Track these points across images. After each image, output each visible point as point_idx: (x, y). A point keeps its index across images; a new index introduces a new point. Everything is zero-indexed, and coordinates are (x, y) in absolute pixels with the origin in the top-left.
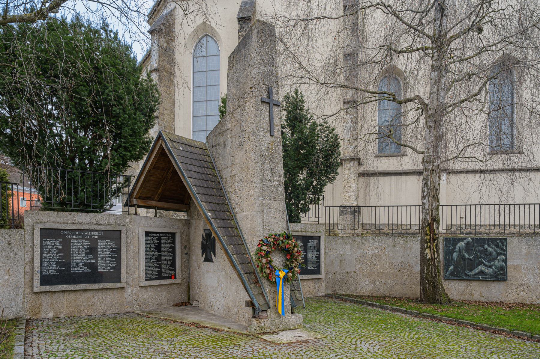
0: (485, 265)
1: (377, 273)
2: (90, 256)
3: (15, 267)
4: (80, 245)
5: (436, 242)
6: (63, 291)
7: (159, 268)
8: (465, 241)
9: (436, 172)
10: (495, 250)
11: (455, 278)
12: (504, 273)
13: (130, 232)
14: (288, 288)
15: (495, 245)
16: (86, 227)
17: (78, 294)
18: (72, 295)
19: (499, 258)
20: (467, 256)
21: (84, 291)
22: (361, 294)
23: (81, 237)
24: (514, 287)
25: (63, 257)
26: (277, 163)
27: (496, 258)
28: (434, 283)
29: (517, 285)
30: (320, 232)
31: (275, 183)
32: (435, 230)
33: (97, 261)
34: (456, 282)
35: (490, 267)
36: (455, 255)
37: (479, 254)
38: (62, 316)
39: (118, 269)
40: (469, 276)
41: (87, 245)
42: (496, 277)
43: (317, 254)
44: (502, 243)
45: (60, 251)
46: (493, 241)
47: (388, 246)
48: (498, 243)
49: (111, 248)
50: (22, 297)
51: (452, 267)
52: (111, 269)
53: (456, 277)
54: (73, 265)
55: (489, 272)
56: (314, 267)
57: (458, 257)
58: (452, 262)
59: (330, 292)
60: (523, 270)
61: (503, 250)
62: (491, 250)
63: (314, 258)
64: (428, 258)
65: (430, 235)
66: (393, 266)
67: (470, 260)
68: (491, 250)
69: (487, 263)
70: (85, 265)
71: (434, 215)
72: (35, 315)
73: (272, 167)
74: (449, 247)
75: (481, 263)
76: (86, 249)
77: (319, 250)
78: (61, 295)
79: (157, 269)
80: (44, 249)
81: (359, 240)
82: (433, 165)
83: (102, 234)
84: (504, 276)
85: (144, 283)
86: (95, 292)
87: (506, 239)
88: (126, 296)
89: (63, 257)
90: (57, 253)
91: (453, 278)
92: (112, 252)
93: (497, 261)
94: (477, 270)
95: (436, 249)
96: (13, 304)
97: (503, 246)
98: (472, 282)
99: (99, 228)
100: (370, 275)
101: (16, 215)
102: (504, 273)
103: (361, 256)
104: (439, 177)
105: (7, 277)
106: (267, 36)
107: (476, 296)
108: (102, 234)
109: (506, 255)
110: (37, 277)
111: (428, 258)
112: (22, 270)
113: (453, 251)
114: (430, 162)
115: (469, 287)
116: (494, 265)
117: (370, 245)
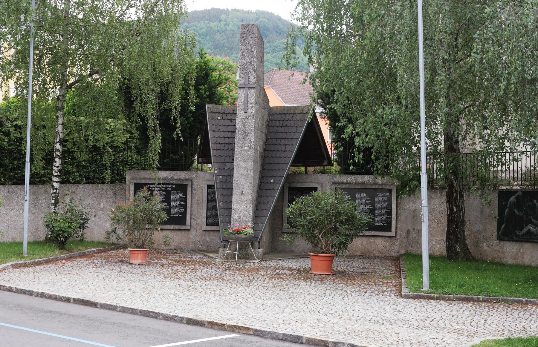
2: (166, 204)
8: (516, 195)
13: (196, 186)
39: (184, 214)
41: (164, 195)
43: (387, 209)
49: (180, 198)
52: (180, 214)
56: (383, 223)
63: (383, 213)
76: (163, 199)
83: (174, 186)
85: (205, 227)
92: (181, 201)
94: (525, 230)
99: (172, 182)
101: (274, 154)
115: (522, 250)
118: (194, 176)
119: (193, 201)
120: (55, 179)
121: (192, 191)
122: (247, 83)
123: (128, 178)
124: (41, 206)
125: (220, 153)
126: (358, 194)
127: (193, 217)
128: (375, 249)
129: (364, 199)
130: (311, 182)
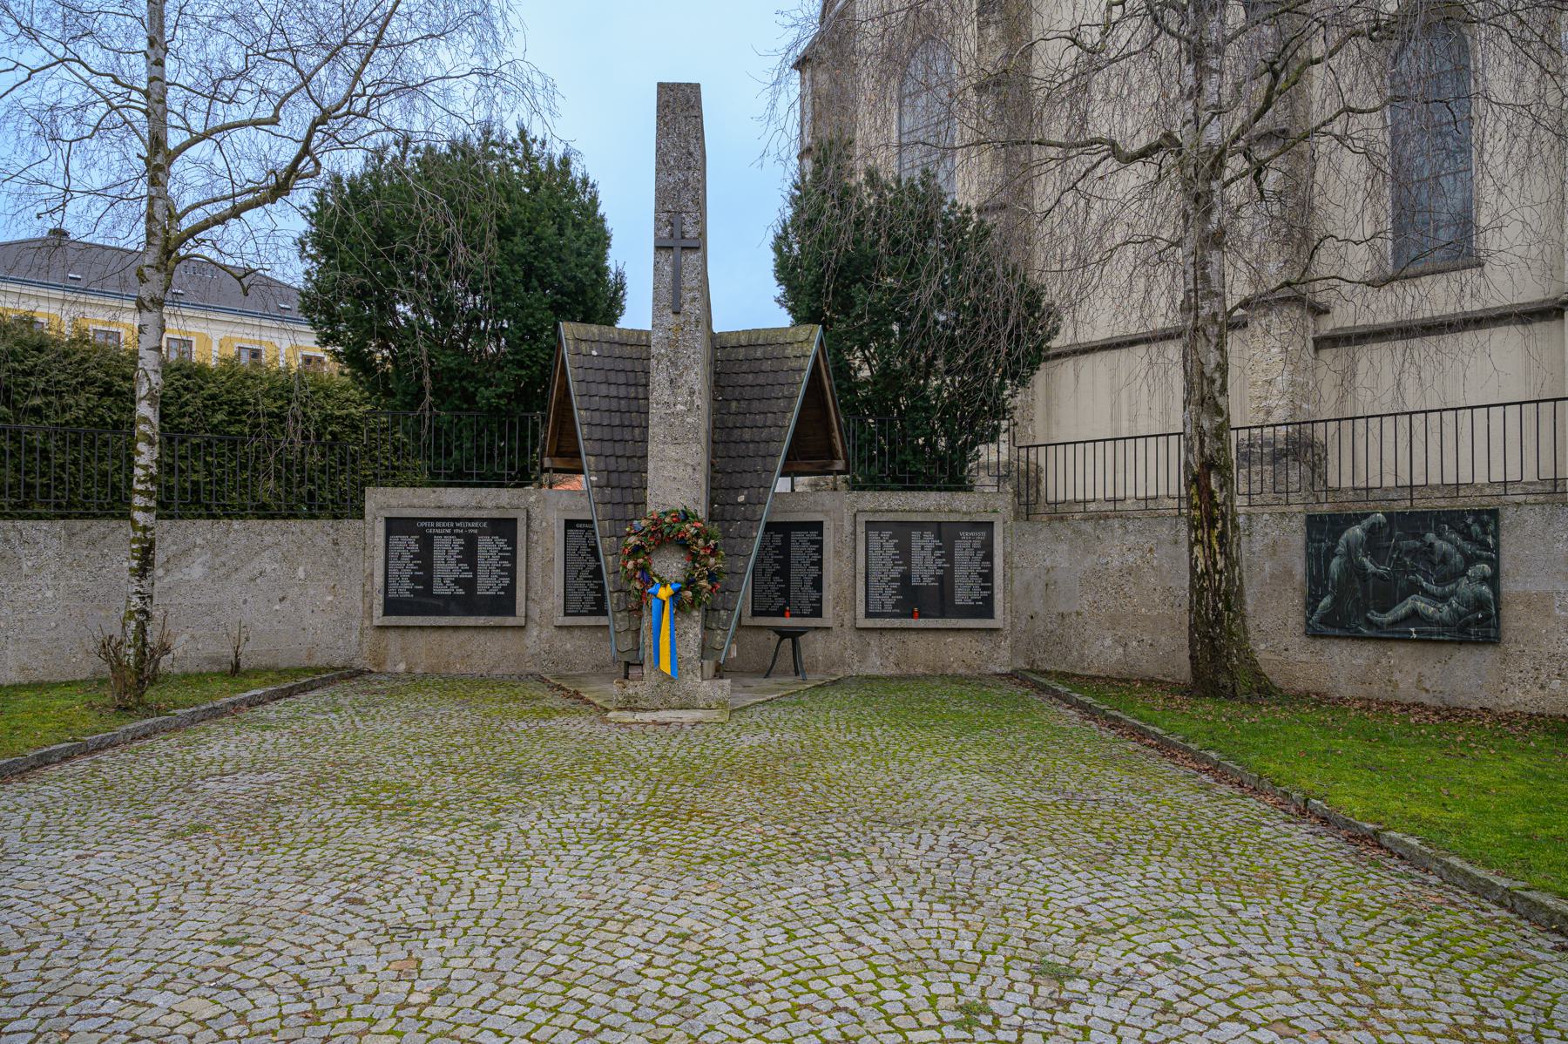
0: (1426, 593)
1: (1131, 617)
2: (465, 566)
3: (346, 582)
4: (447, 546)
5: (1219, 525)
6: (421, 628)
7: (597, 591)
8: (1365, 523)
9: (1205, 335)
10: (1458, 548)
11: (1337, 632)
12: (1488, 617)
14: (697, 622)
15: (1460, 532)
16: (456, 514)
17: (445, 635)
18: (436, 636)
19: (1470, 572)
20: (1371, 567)
21: (456, 628)
22: (1093, 672)
23: (449, 531)
24: (1527, 664)
25: (421, 568)
26: (686, 368)
27: (1463, 573)
28: (1212, 639)
29: (1539, 656)
30: (995, 511)
31: (680, 407)
32: (1213, 492)
33: (475, 575)
34: (1344, 643)
35: (1444, 599)
36: (1335, 564)
37: (1408, 560)
38: (418, 671)
39: (511, 590)
40: (1378, 626)
42: (1463, 629)
44: (1483, 525)
45: (416, 556)
46: (1452, 519)
47: (1160, 543)
48: (1468, 527)
50: (357, 633)
51: (1326, 601)
53: (1341, 628)
54: (437, 581)
55: (1438, 615)
56: (974, 600)
57: (1344, 570)
58: (1327, 586)
59: (1021, 664)
60: (1557, 611)
61: (1486, 547)
62: (1446, 546)
63: (974, 576)
64: (1199, 570)
65: (1200, 508)
66: (1172, 599)
67: (1381, 577)
68: (1446, 546)
69: (1433, 588)
70: (456, 581)
71: (1207, 451)
72: (378, 665)
73: (673, 376)
74: (1320, 541)
75: (1415, 588)
77: (989, 557)
78: (417, 633)
79: (593, 595)
80: (391, 554)
81: (1090, 530)
82: (1197, 317)
83: (485, 525)
84: (1490, 626)
86: (474, 633)
87: (1494, 514)
88: (529, 642)
89: (421, 568)
90: (411, 560)
91: (1330, 631)
92: (502, 558)
93: (1464, 581)
94: (1401, 610)
95: (1221, 545)
96: (340, 642)
97: (1485, 533)
98: (1391, 644)
99: (477, 514)
100: (1114, 622)
102: (1488, 617)
103: (1094, 572)
104: (1221, 347)
105: (330, 598)
106: (678, 110)
107: (1406, 689)
108: (485, 525)
109: (1495, 564)
110: (379, 600)
111: (1199, 570)
112: (359, 588)
113: (1331, 553)
114: (1190, 310)
115: (1384, 661)
116: (1453, 593)
117: (1116, 542)
118: (532, 499)
119: (532, 559)
120: (138, 501)
121: (528, 535)
122: (677, 235)
123: (369, 506)
124: (116, 576)
125: (597, 433)
126: (915, 535)
127: (532, 595)
128: (956, 659)
129: (929, 546)
130: (807, 510)
